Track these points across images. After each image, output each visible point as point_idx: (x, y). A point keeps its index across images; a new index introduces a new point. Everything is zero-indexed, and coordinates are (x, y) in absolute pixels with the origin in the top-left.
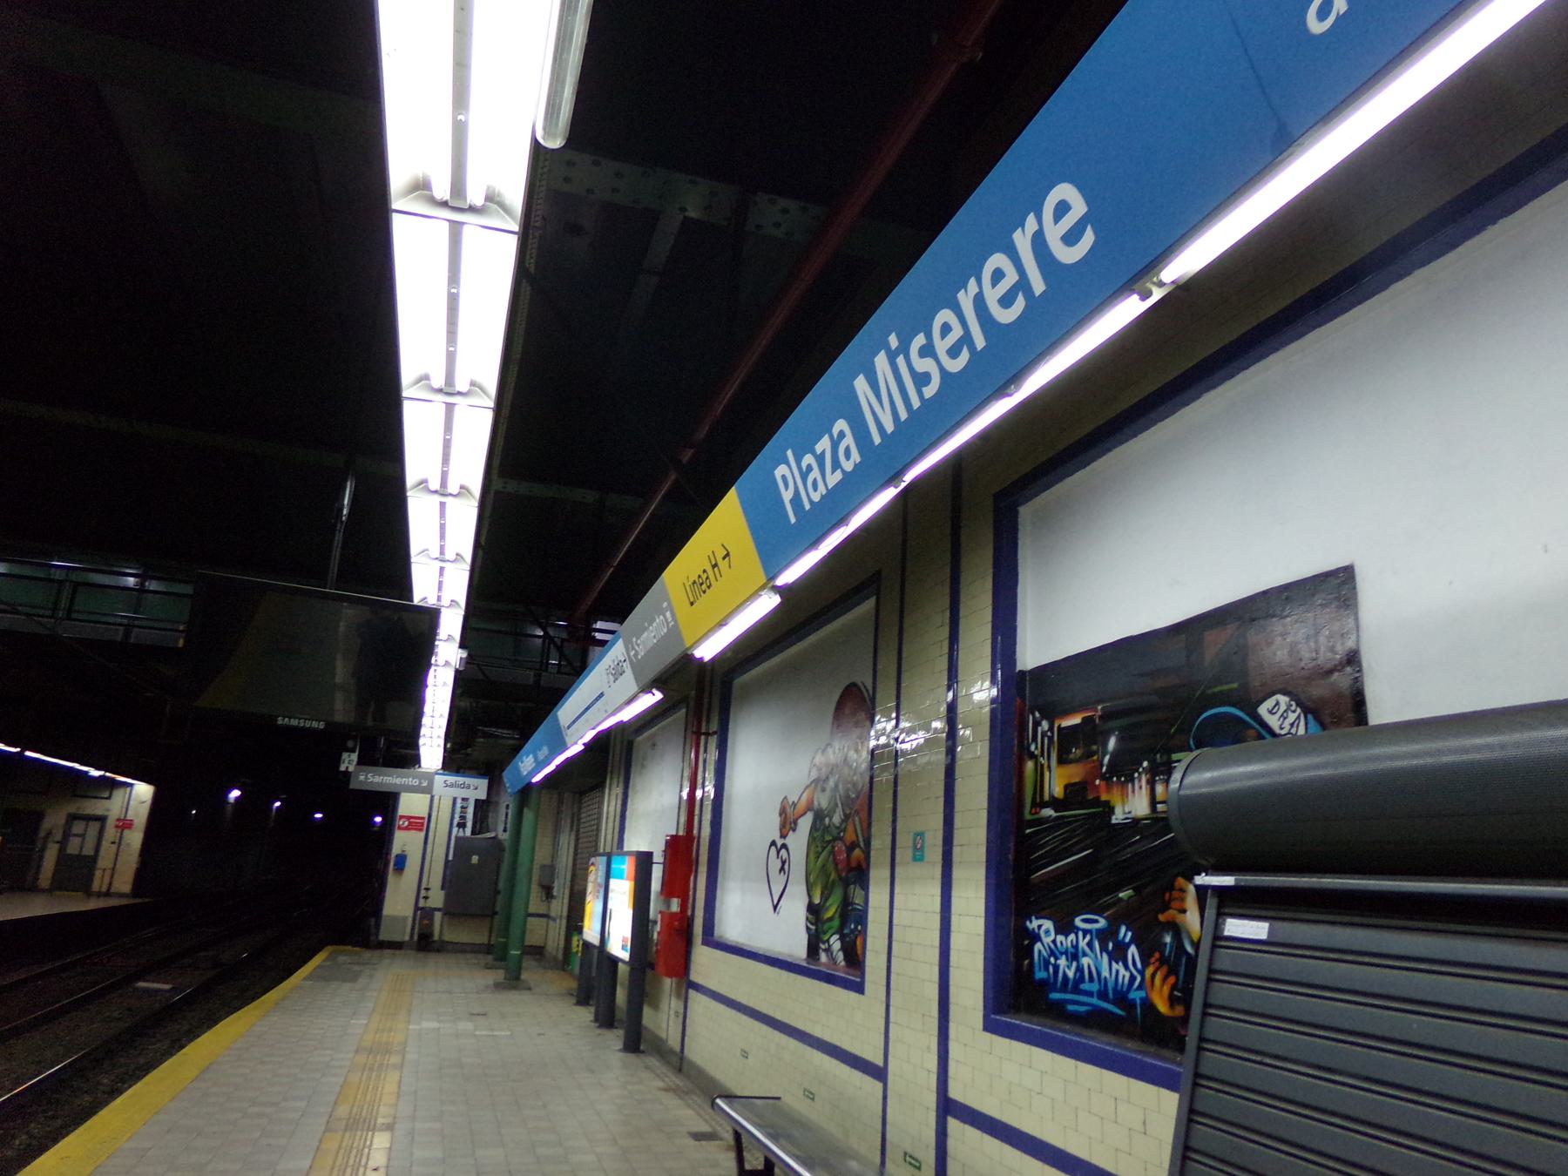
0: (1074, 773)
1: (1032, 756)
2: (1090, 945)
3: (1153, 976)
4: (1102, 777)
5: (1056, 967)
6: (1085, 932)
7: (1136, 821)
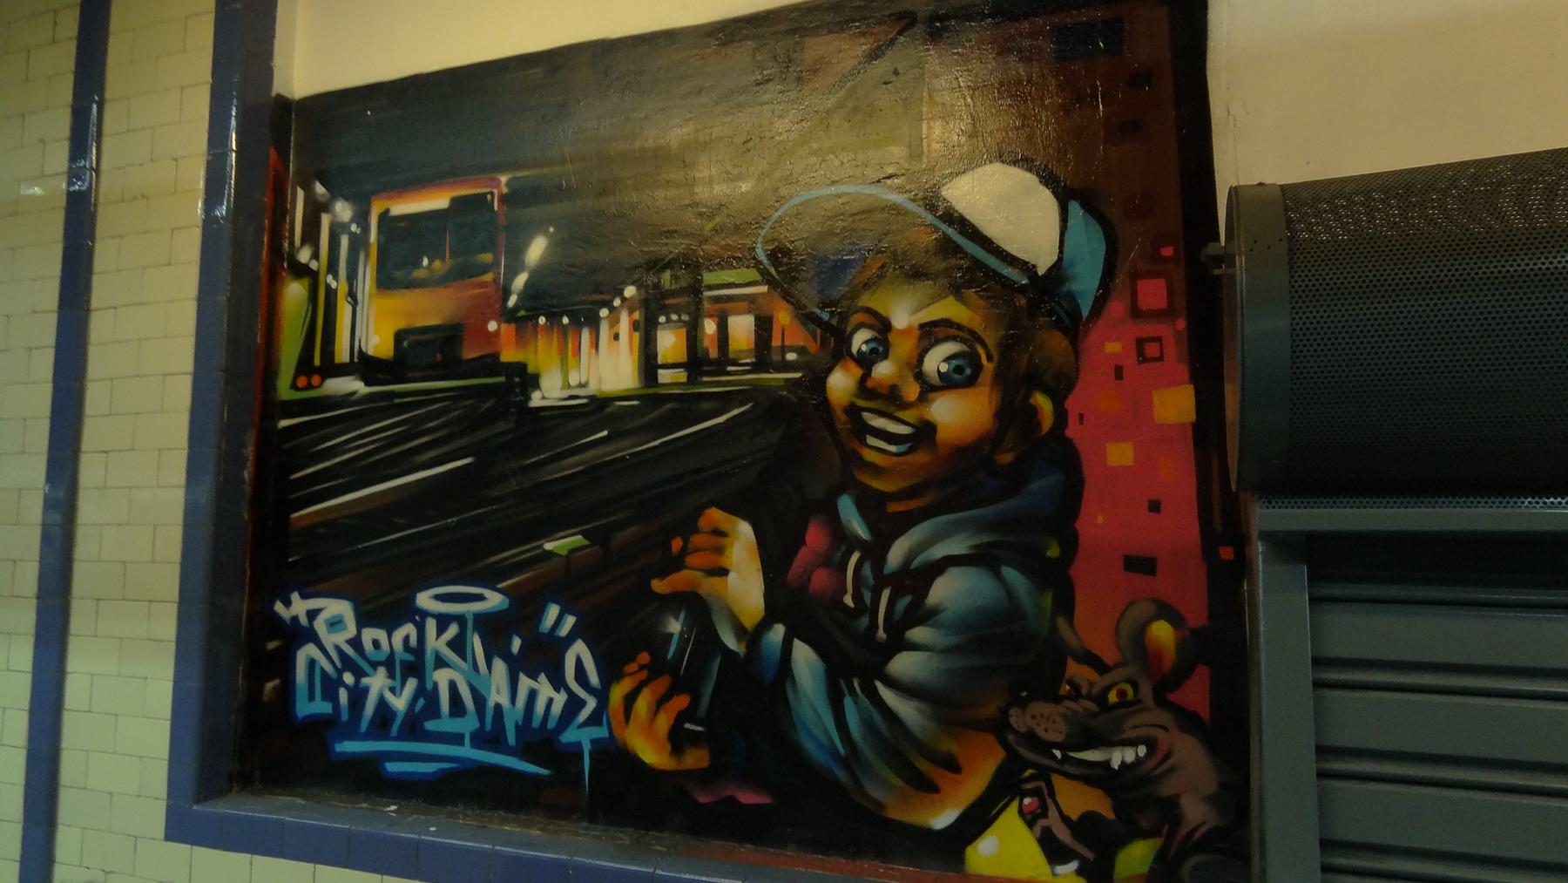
0: (427, 308)
1: (301, 271)
2: (458, 645)
3: (630, 699)
4: (509, 316)
5: (358, 695)
6: (443, 621)
7: (599, 406)
